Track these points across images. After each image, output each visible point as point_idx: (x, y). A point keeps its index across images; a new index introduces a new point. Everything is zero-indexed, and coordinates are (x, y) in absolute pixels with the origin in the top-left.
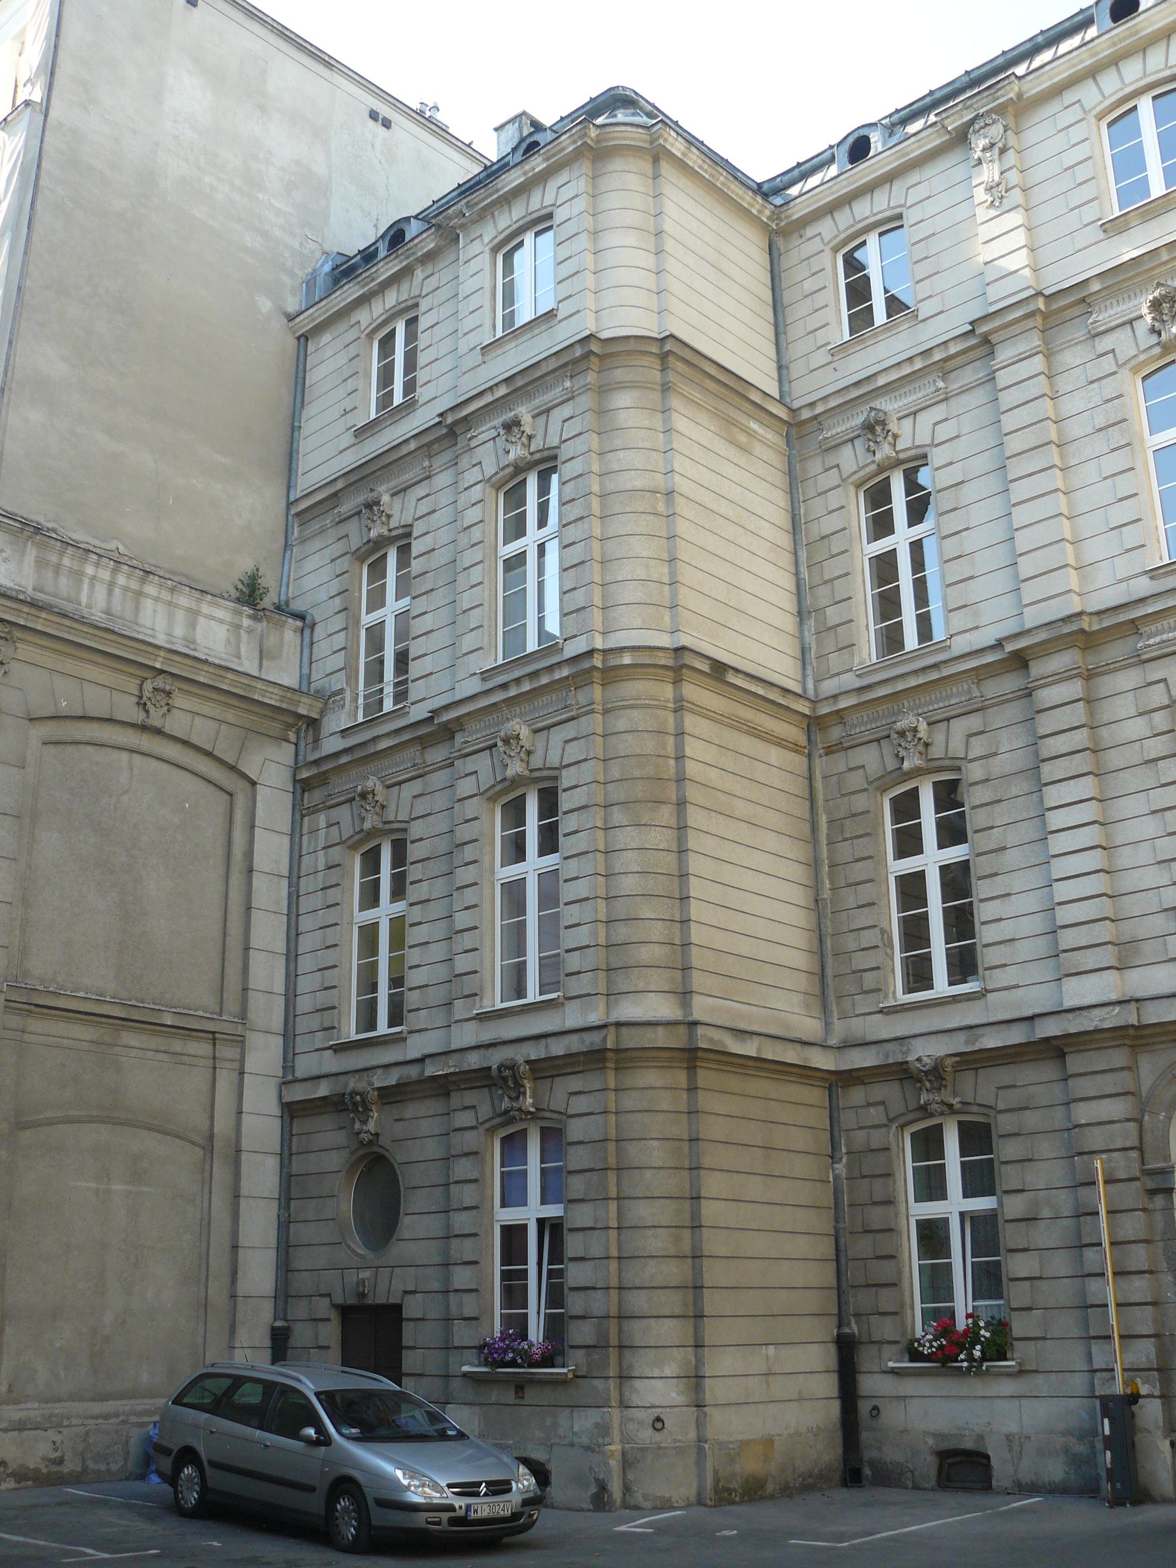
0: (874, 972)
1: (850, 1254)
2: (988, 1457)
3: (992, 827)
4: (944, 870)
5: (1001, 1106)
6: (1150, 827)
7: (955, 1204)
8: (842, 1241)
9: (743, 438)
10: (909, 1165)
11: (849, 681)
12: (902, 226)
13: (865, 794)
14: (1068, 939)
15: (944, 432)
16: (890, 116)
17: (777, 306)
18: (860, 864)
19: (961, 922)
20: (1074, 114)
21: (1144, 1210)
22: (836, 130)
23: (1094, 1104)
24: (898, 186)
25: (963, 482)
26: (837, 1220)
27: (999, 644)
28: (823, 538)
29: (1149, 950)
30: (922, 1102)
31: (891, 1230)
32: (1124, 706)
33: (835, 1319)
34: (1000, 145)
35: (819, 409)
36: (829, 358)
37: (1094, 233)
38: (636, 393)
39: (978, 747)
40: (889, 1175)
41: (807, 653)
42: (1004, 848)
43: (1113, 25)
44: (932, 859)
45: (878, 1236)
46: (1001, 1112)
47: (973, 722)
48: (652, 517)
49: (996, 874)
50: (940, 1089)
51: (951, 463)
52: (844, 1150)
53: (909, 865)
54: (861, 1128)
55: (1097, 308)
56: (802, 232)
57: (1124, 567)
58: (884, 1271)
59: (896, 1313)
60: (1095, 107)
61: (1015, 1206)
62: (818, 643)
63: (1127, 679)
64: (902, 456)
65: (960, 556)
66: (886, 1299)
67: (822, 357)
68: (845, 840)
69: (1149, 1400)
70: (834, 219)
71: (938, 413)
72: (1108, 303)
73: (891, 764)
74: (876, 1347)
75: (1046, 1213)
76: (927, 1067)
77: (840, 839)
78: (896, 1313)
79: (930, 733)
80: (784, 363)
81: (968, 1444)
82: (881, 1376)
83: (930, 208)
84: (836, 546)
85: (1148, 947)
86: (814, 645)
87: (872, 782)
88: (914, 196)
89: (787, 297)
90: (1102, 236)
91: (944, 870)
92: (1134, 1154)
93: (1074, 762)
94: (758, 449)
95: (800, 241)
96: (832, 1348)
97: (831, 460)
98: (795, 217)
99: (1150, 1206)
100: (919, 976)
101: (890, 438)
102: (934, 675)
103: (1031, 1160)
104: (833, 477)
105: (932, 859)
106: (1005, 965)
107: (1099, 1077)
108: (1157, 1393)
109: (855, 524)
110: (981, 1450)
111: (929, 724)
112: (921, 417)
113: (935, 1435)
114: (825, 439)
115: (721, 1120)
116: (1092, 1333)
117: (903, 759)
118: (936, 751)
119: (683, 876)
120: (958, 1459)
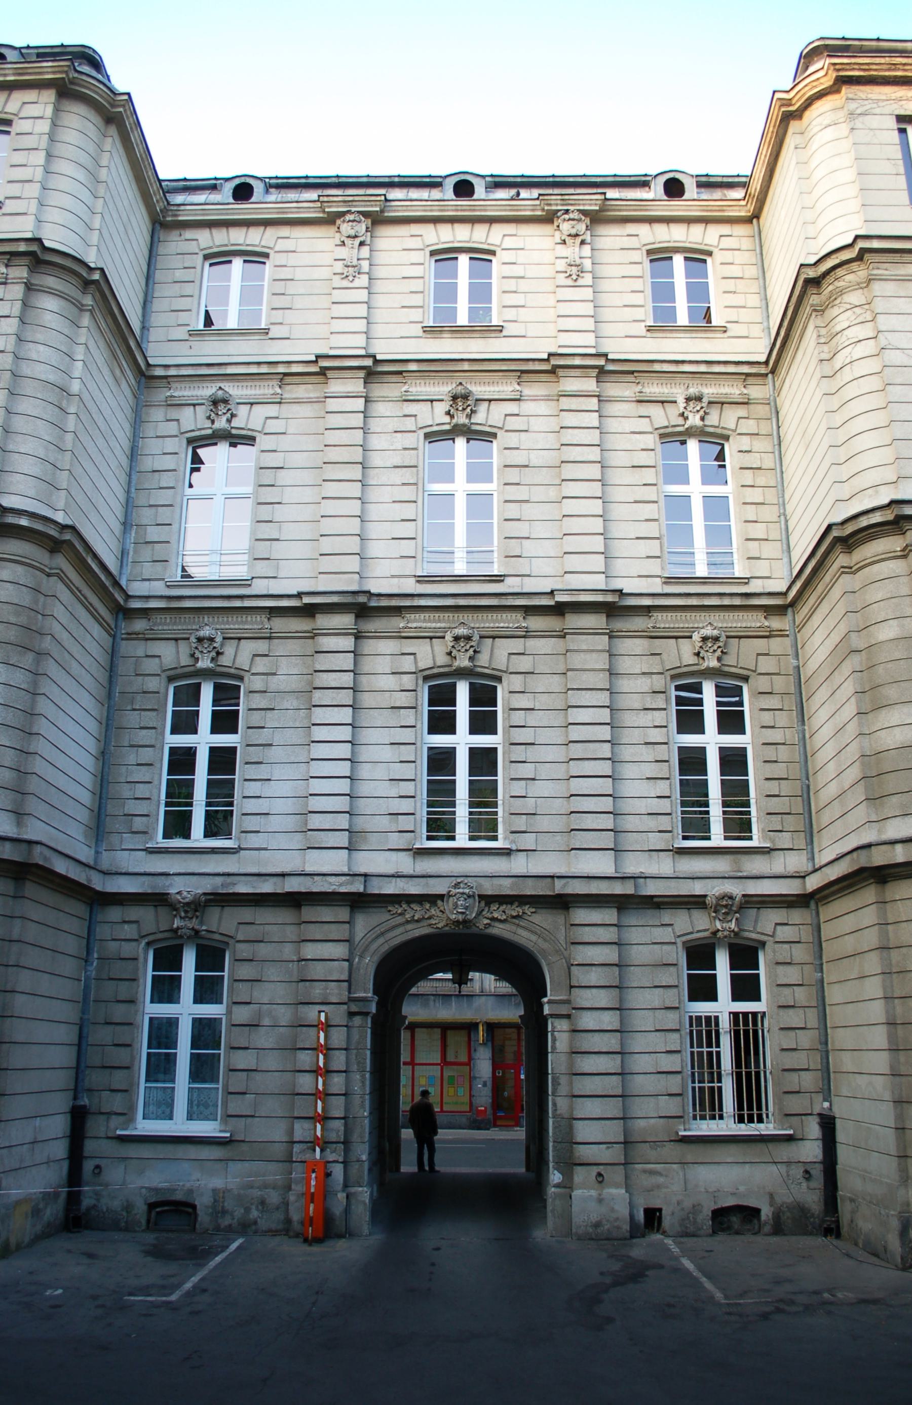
0: (144, 818)
1: (91, 1040)
2: (194, 1207)
3: (263, 727)
4: (213, 751)
5: (240, 937)
6: (387, 753)
7: (186, 1010)
8: (85, 1030)
9: (118, 372)
10: (150, 973)
11: (158, 588)
12: (264, 263)
13: (158, 678)
14: (316, 821)
15: (272, 426)
16: (270, 178)
17: (149, 278)
18: (144, 732)
19: (221, 791)
20: (416, 243)
21: (346, 1026)
22: (228, 166)
23: (319, 946)
24: (271, 232)
25: (282, 468)
26: (83, 1012)
27: (299, 595)
28: (154, 471)
29: (374, 841)
30: (175, 926)
31: (131, 1024)
32: (383, 665)
33: (72, 1093)
34: (362, 239)
35: (172, 372)
36: (187, 337)
37: (417, 330)
38: (63, 303)
39: (261, 665)
40: (134, 980)
41: (125, 556)
42: (271, 745)
43: (454, 198)
44: (204, 740)
45: (118, 1028)
46: (239, 941)
47: (261, 646)
48: (57, 410)
49: (261, 763)
50: (192, 918)
51: (275, 451)
52: (96, 956)
53: (183, 740)
54: (113, 940)
55: (409, 382)
56: (182, 232)
57: (396, 567)
58: (120, 1056)
59: (126, 1091)
60: (432, 245)
61: (242, 1014)
62: (135, 552)
63: (387, 646)
64: (234, 432)
65: (271, 521)
66: (118, 1079)
67: (181, 333)
68: (134, 710)
69: (334, 1165)
70: (211, 234)
71: (272, 410)
72: (418, 382)
73: (185, 660)
74: (103, 1117)
75: (266, 1021)
76: (187, 900)
77: (129, 708)
78: (126, 1091)
79: (222, 645)
80: (147, 325)
81: (179, 1196)
82: (105, 1141)
83: (292, 259)
84: (166, 480)
85: (373, 838)
86: (131, 553)
87: (165, 671)
88: (282, 245)
89: (159, 276)
90: (421, 333)
91: (213, 751)
92: (346, 984)
93: (340, 695)
94: (124, 385)
95: (179, 239)
96: (69, 1116)
97: (173, 413)
98: (180, 218)
99: (350, 1024)
100: (178, 824)
101: (229, 415)
102: (238, 603)
103: (260, 981)
104: (172, 428)
105: (204, 740)
106: (258, 832)
107: (326, 926)
108: (341, 1159)
109: (182, 469)
110: (190, 1201)
111: (224, 638)
112: (256, 408)
113: (149, 1189)
114: (172, 396)
115: (34, 925)
116: (296, 1114)
117: (198, 659)
118: (226, 660)
119: (31, 714)
120: (166, 1208)
